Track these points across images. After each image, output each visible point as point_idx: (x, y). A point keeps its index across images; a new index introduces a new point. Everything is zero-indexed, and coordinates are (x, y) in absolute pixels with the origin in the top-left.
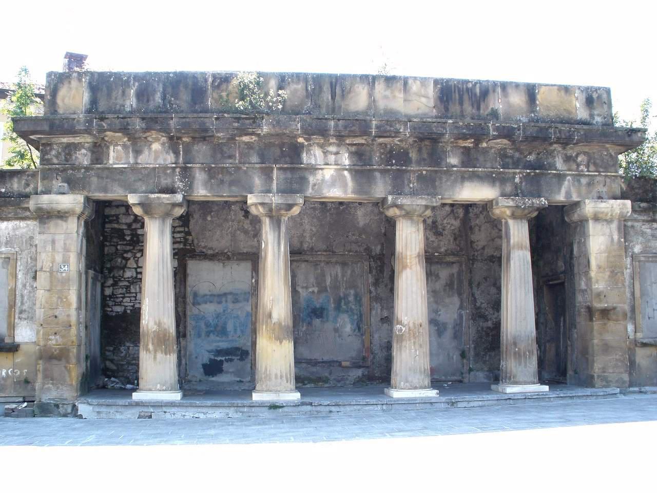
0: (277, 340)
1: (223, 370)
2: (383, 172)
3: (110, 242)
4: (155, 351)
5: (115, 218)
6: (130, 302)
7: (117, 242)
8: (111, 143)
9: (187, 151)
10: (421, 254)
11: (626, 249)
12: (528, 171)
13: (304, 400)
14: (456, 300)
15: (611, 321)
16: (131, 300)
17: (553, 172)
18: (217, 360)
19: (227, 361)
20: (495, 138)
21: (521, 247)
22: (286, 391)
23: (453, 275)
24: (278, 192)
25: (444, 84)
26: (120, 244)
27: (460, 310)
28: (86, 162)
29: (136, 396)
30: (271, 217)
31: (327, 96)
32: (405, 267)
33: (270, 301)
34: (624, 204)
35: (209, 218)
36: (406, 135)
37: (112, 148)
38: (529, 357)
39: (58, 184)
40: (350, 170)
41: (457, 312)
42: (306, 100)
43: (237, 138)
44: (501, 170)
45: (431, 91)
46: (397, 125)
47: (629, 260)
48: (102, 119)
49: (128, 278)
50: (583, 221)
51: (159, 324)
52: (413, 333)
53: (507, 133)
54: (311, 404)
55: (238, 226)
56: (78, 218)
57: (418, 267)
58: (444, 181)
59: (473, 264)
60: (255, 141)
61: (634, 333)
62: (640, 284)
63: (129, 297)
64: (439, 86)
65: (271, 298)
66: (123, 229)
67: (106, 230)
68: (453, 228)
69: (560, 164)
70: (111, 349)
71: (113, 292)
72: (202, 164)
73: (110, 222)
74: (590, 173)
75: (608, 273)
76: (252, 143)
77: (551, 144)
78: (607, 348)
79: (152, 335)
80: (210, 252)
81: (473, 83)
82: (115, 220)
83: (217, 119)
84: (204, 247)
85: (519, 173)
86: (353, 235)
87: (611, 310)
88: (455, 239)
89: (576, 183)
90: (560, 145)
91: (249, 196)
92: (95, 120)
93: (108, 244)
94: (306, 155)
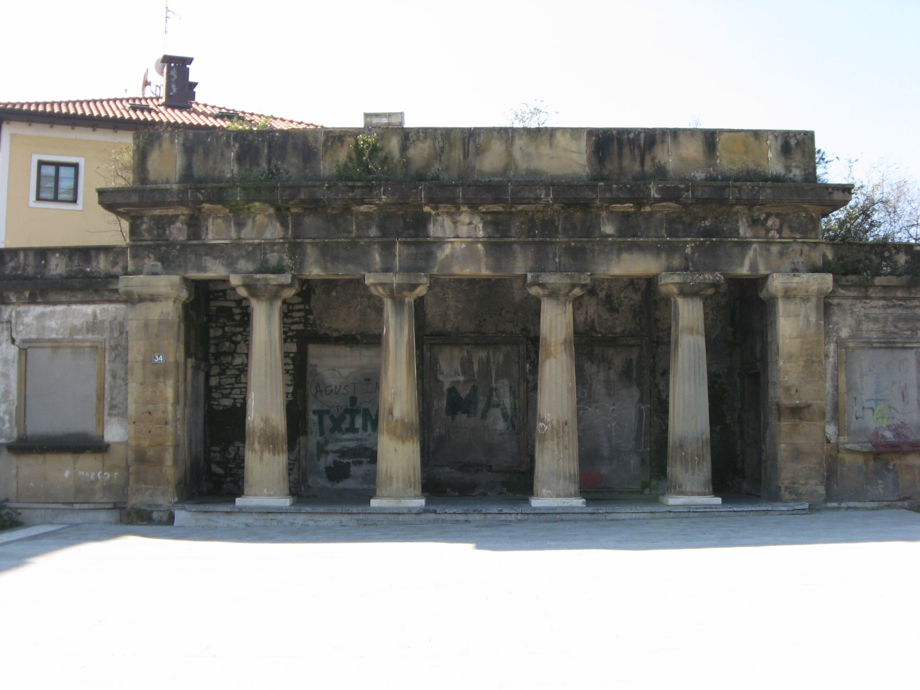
0: (399, 439)
1: (350, 475)
2: (524, 245)
3: (216, 323)
4: (262, 451)
5: (221, 294)
6: (240, 394)
7: (225, 323)
8: (209, 216)
9: (298, 224)
10: (568, 340)
11: (827, 333)
12: (702, 239)
13: (428, 508)
14: (635, 393)
15: (803, 422)
16: (241, 392)
17: (733, 239)
18: (342, 463)
19: (355, 463)
20: (657, 201)
21: (691, 331)
22: (410, 497)
23: (631, 360)
24: (400, 271)
25: (601, 136)
26: (228, 326)
27: (640, 405)
28: (182, 238)
29: (239, 501)
30: (393, 298)
31: (458, 154)
32: (548, 355)
33: (391, 395)
34: (823, 279)
35: (334, 294)
36: (548, 201)
37: (211, 220)
38: (699, 462)
39: (150, 262)
40: (485, 244)
41: (636, 407)
42: (434, 161)
43: (353, 208)
44: (668, 239)
45: (583, 144)
46: (538, 191)
47: (832, 347)
48: (198, 190)
49: (238, 365)
50: (773, 300)
51: (266, 421)
52: (557, 433)
53: (670, 194)
54: (435, 512)
55: (368, 303)
56: (175, 302)
57: (564, 357)
58: (596, 254)
59: (657, 347)
60: (374, 211)
61: (836, 436)
62: (846, 376)
63: (240, 388)
64: (594, 139)
65: (393, 391)
66: (231, 308)
67: (211, 308)
68: (632, 303)
69: (744, 230)
70: (218, 449)
71: (219, 382)
72: (315, 238)
73: (216, 299)
74: (782, 240)
75: (802, 363)
76: (371, 213)
77: (732, 206)
78: (797, 454)
79: (258, 434)
80: (335, 334)
81: (637, 132)
82: (221, 297)
83: (328, 188)
84: (329, 328)
85: (691, 242)
86: (507, 312)
87: (804, 408)
88: (634, 317)
89: (764, 253)
90: (745, 207)
91: (367, 275)
92: (189, 191)
93: (213, 325)
94: (434, 226)
